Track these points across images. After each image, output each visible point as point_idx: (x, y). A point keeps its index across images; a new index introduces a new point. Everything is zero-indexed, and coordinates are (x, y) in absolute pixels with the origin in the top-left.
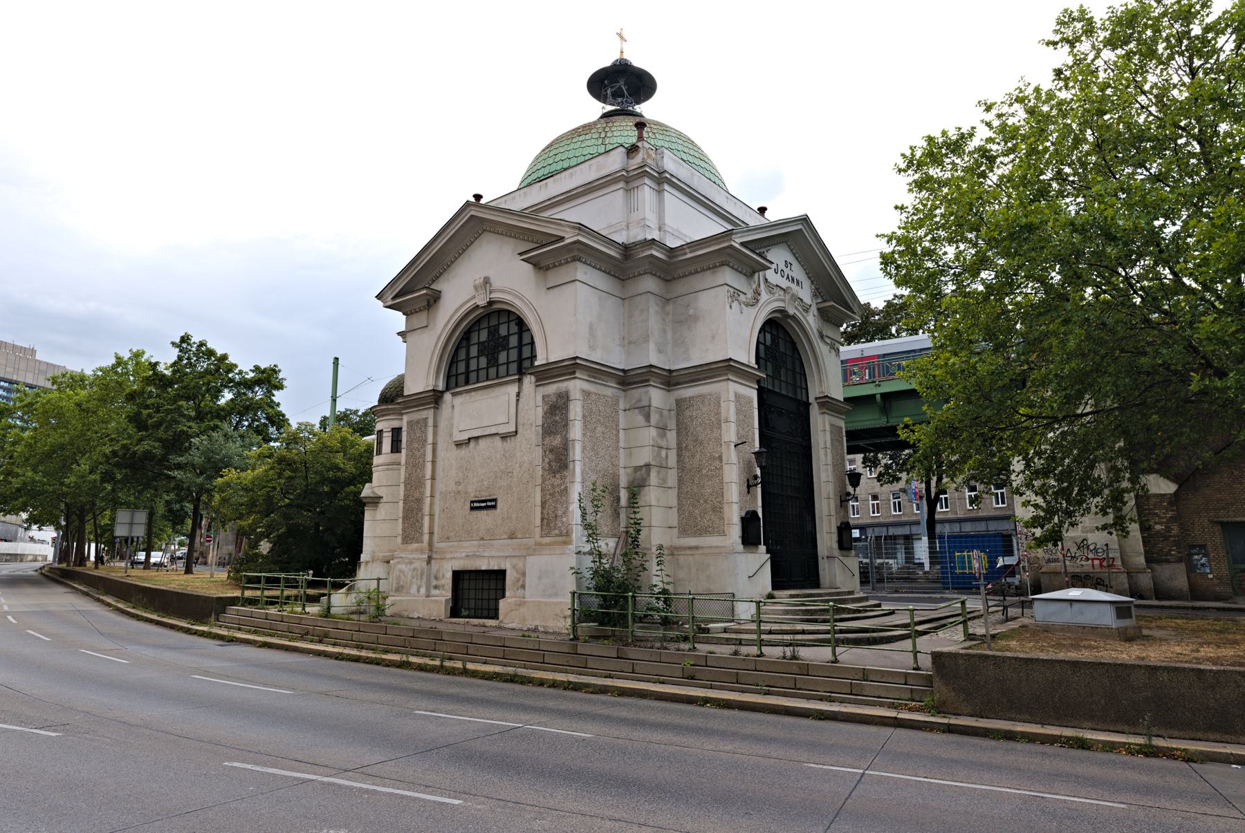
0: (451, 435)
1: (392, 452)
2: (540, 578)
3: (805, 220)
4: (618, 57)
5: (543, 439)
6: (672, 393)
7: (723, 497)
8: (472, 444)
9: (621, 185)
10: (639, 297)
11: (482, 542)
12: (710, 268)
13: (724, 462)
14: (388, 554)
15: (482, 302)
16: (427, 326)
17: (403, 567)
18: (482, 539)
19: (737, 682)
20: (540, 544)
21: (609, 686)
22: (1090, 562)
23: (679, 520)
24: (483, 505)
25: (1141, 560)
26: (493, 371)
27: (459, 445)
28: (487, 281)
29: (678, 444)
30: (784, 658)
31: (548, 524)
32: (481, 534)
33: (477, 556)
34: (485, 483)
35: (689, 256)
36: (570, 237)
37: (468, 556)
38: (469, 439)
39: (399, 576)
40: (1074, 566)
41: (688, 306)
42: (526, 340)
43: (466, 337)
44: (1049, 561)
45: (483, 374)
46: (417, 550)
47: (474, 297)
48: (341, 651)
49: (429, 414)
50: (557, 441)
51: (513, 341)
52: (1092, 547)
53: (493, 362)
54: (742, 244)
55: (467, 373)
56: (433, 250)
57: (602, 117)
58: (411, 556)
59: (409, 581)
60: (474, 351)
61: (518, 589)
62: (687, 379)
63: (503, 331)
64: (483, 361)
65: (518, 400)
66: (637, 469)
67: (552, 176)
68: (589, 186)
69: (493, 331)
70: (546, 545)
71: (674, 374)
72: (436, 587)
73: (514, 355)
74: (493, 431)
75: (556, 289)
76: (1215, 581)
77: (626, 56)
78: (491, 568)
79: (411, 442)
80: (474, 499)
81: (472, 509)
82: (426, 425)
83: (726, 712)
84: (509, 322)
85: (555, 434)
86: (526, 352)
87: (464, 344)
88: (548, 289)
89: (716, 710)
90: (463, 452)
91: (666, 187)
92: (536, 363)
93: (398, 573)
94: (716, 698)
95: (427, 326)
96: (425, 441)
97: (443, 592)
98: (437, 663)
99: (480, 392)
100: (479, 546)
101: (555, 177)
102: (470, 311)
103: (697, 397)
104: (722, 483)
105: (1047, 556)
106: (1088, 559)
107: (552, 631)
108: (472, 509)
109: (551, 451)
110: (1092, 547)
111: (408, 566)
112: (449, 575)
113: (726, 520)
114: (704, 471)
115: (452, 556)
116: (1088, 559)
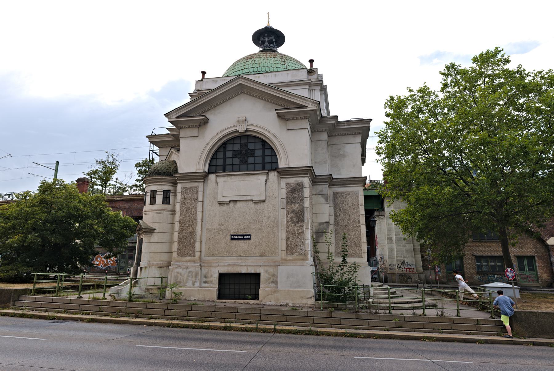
0: (215, 198)
1: (163, 203)
2: (288, 277)
5: (287, 205)
6: (331, 189)
7: (361, 240)
8: (232, 204)
9: (307, 87)
10: (321, 142)
11: (239, 257)
12: (352, 134)
13: (361, 223)
14: (160, 263)
16: (197, 136)
18: (240, 256)
19: (423, 328)
20: (286, 260)
21: (371, 334)
22: (406, 269)
23: (336, 250)
24: (241, 237)
25: (421, 269)
27: (221, 204)
29: (334, 213)
30: (438, 315)
31: (291, 250)
32: (239, 253)
33: (237, 265)
34: (242, 226)
35: (346, 127)
37: (228, 265)
38: (230, 201)
39: (177, 276)
40: (400, 271)
41: (340, 149)
43: (224, 145)
44: (391, 269)
46: (190, 261)
47: (236, 126)
48: (171, 322)
49: (200, 185)
50: (297, 207)
51: (259, 153)
52: (406, 264)
56: (210, 96)
57: (259, 52)
58: (186, 264)
59: (185, 279)
60: (229, 154)
61: (269, 283)
62: (339, 183)
63: (251, 146)
65: (266, 184)
66: (321, 224)
67: (263, 73)
68: (289, 83)
70: (290, 260)
71: (334, 180)
72: (205, 282)
73: (259, 160)
75: (293, 131)
76: (442, 277)
78: (249, 272)
79: (185, 199)
80: (233, 234)
81: (232, 239)
82: (197, 191)
85: (295, 203)
88: (288, 130)
89: (433, 342)
90: (225, 208)
92: (155, 162)
93: (175, 274)
95: (197, 136)
96: (197, 199)
97: (211, 285)
98: (272, 327)
99: (238, 177)
100: (238, 260)
101: (265, 74)
102: (228, 134)
103: (345, 192)
104: (360, 233)
105: (390, 267)
106: (405, 268)
107: (298, 305)
108: (232, 239)
109: (292, 212)
110: (406, 264)
111: (185, 270)
112: (217, 275)
113: (363, 250)
114: (350, 227)
115: (217, 264)
116: (405, 268)
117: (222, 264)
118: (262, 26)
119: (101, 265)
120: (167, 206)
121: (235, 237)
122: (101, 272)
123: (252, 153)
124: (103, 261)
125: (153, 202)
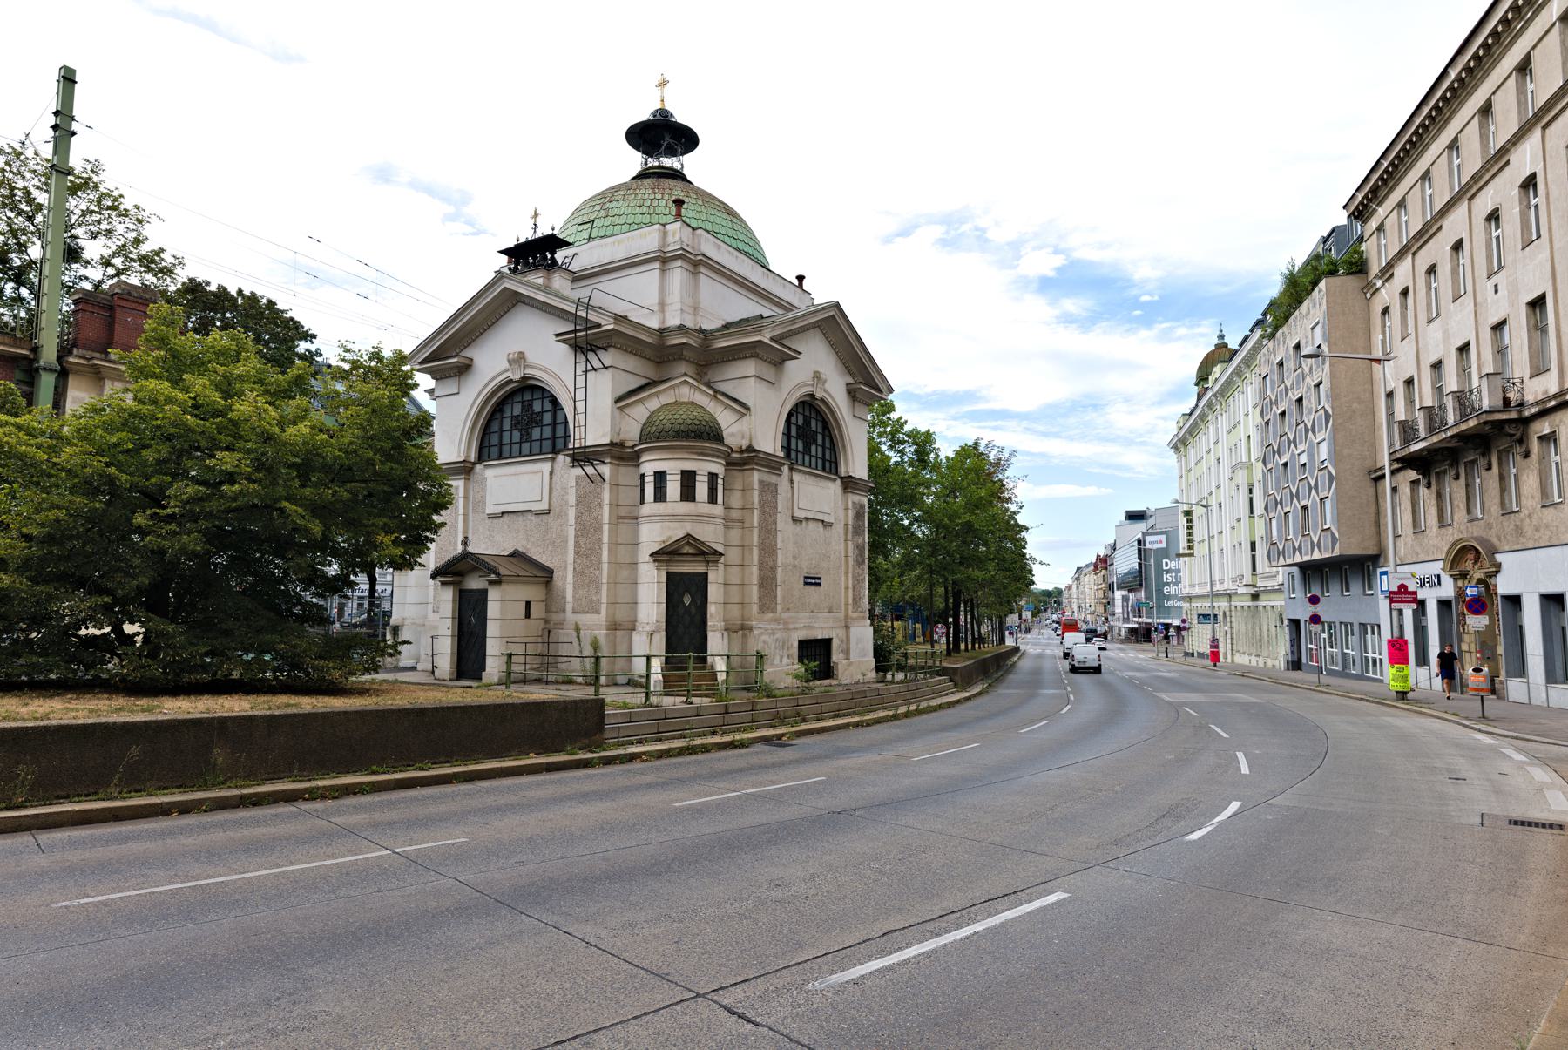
1: (655, 501)
3: (837, 305)
9: (657, 265)
15: (517, 376)
17: (765, 637)
18: (812, 612)
26: (526, 446)
28: (521, 356)
38: (503, 513)
42: (560, 419)
45: (516, 448)
47: (507, 371)
51: (547, 418)
53: (526, 437)
54: (772, 339)
55: (501, 445)
60: (507, 424)
63: (537, 407)
64: (517, 435)
65: (551, 479)
69: (527, 407)
73: (547, 432)
74: (821, 517)
84: (542, 399)
86: (560, 431)
87: (498, 415)
90: (798, 528)
91: (702, 269)
94: (68, 725)
99: (813, 477)
108: (806, 583)
112: (796, 644)
117: (797, 626)
118: (644, 115)
120: (661, 505)
121: (528, 615)
123: (536, 420)
125: (660, 495)
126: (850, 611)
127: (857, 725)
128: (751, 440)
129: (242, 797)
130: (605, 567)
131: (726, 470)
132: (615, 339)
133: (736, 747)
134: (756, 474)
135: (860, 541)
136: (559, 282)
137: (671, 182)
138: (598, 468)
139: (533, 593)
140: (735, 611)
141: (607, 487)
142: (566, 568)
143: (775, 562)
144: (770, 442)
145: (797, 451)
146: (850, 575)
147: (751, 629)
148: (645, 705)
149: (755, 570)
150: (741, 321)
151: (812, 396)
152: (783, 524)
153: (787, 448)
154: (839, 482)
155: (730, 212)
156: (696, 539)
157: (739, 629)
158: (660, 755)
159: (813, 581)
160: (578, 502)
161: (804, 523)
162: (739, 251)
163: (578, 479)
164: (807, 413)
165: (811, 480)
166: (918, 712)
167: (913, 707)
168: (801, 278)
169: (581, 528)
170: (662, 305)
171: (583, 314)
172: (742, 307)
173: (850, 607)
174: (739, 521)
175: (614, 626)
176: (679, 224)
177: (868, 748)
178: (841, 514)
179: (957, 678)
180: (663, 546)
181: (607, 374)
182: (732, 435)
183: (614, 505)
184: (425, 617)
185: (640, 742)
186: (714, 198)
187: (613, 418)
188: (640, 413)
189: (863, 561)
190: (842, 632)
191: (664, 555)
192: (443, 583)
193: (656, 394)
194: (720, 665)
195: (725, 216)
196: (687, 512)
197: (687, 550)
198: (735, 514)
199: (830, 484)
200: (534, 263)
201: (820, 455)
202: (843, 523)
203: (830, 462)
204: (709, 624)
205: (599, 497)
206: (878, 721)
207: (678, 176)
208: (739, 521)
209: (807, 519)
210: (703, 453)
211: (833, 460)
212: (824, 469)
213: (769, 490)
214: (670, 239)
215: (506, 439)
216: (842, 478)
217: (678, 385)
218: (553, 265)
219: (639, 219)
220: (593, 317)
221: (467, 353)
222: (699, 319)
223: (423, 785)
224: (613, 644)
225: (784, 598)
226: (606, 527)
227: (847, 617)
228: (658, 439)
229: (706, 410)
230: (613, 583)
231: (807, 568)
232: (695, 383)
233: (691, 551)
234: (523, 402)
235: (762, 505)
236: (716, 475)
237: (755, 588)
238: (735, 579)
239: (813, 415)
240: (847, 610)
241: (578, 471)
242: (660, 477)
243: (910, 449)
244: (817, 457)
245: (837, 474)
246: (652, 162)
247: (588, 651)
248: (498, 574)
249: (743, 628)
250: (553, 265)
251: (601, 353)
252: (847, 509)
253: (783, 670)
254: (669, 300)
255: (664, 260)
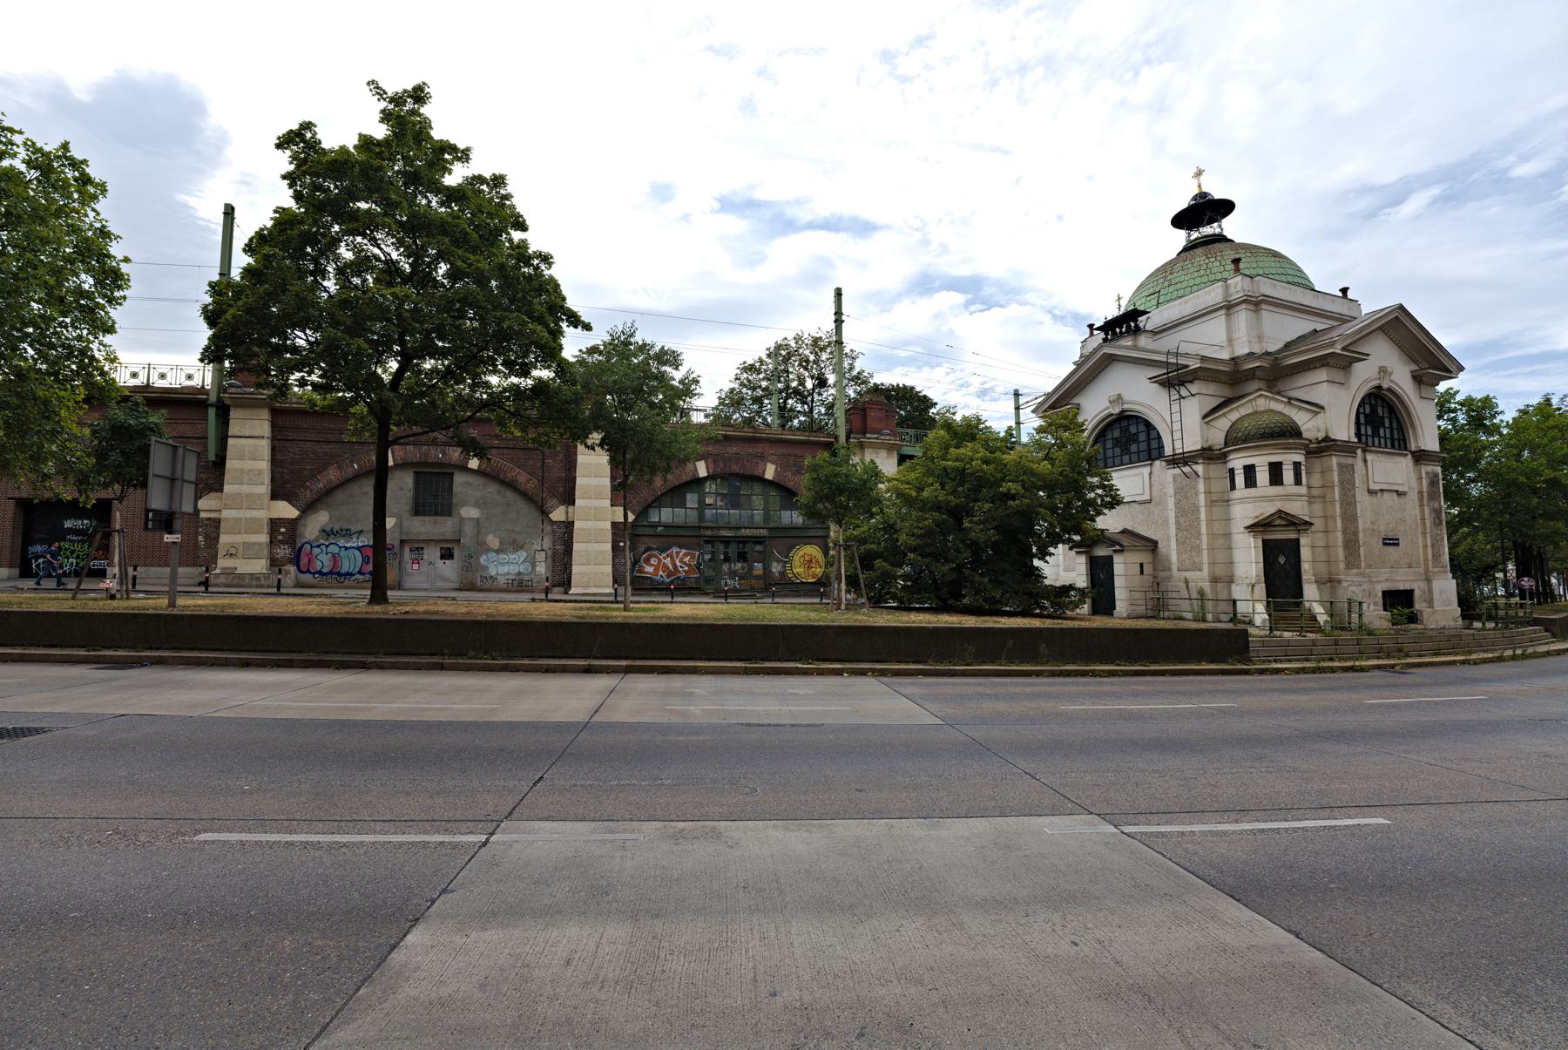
1: (1246, 487)
3: (1401, 308)
4: (1196, 191)
9: (1223, 312)
15: (1117, 411)
17: (1354, 588)
26: (1126, 458)
28: (1119, 397)
36: (1194, 364)
51: (1142, 437)
54: (1343, 349)
60: (1109, 444)
63: (1133, 430)
64: (1118, 451)
69: (1125, 431)
73: (1143, 446)
74: (1395, 488)
77: (1204, 189)
81: (1385, 544)
83: (1116, 679)
86: (1154, 444)
90: (1374, 499)
91: (1264, 306)
99: (1384, 456)
108: (1385, 544)
112: (1380, 594)
117: (1380, 579)
118: (1183, 204)
119: (661, 573)
121: (1142, 573)
122: (662, 589)
123: (1134, 439)
124: (665, 566)
126: (1430, 566)
127: (1463, 662)
128: (1327, 432)
129: (1061, 671)
130: (1204, 538)
131: (1306, 458)
132: (1199, 374)
133: (1357, 671)
134: (1334, 458)
135: (1436, 505)
136: (1143, 341)
137: (1218, 245)
138: (1193, 467)
139: (1144, 557)
140: (1323, 568)
141: (1201, 481)
142: (1168, 540)
143: (1357, 527)
144: (1343, 429)
145: (1367, 435)
146: (1428, 536)
147: (1339, 582)
148: (1269, 636)
149: (1339, 535)
150: (1298, 338)
151: (1379, 387)
152: (1361, 497)
153: (1358, 435)
154: (1410, 456)
155: (1276, 255)
156: (1287, 514)
157: (1329, 582)
158: (1298, 671)
159: (1391, 542)
160: (1176, 493)
161: (1379, 494)
162: (1289, 283)
163: (1174, 477)
164: (1373, 402)
165: (1383, 458)
166: (1524, 656)
167: (1519, 652)
168: (1344, 291)
169: (1181, 510)
170: (1230, 341)
171: (1174, 361)
172: (1300, 326)
173: (1430, 563)
174: (1320, 497)
175: (1214, 580)
176: (1240, 278)
177: (1502, 679)
178: (1415, 484)
179: (1556, 629)
180: (1256, 520)
181: (1195, 400)
182: (1308, 430)
183: (1208, 493)
184: (1058, 574)
185: (1275, 661)
186: (1260, 247)
187: (1202, 430)
188: (1223, 423)
189: (1441, 523)
190: (1423, 585)
191: (1256, 528)
192: (1077, 553)
193: (1236, 408)
194: (1318, 609)
195: (1273, 259)
196: (1277, 494)
197: (1278, 522)
198: (1315, 492)
199: (1402, 459)
200: (1121, 332)
201: (1388, 435)
202: (1416, 492)
203: (1399, 440)
204: (1304, 577)
205: (1195, 488)
206: (1485, 661)
207: (1221, 239)
208: (1320, 497)
209: (1382, 490)
210: (1287, 448)
211: (1401, 438)
212: (1393, 447)
213: (1347, 471)
214: (1232, 290)
215: (1109, 453)
216: (1412, 453)
217: (1255, 399)
218: (1137, 330)
219: (1198, 281)
220: (1181, 361)
221: (1075, 401)
222: (1264, 345)
223: (1210, 674)
224: (1215, 591)
225: (1365, 556)
226: (1203, 510)
227: (1427, 571)
228: (1245, 441)
229: (1284, 415)
230: (1211, 548)
231: (1384, 530)
232: (1270, 395)
233: (1283, 523)
234: (1121, 428)
235: (1341, 482)
236: (1300, 463)
237: (1341, 550)
238: (1321, 543)
239: (1379, 403)
240: (1426, 565)
241: (1177, 471)
242: (1250, 471)
243: (1462, 418)
244: (1385, 438)
245: (1406, 449)
246: (1195, 235)
247: (1195, 595)
248: (1121, 545)
249: (1330, 580)
250: (1137, 330)
251: (1189, 386)
252: (1420, 478)
253: (1376, 616)
254: (1235, 336)
255: (1229, 307)
